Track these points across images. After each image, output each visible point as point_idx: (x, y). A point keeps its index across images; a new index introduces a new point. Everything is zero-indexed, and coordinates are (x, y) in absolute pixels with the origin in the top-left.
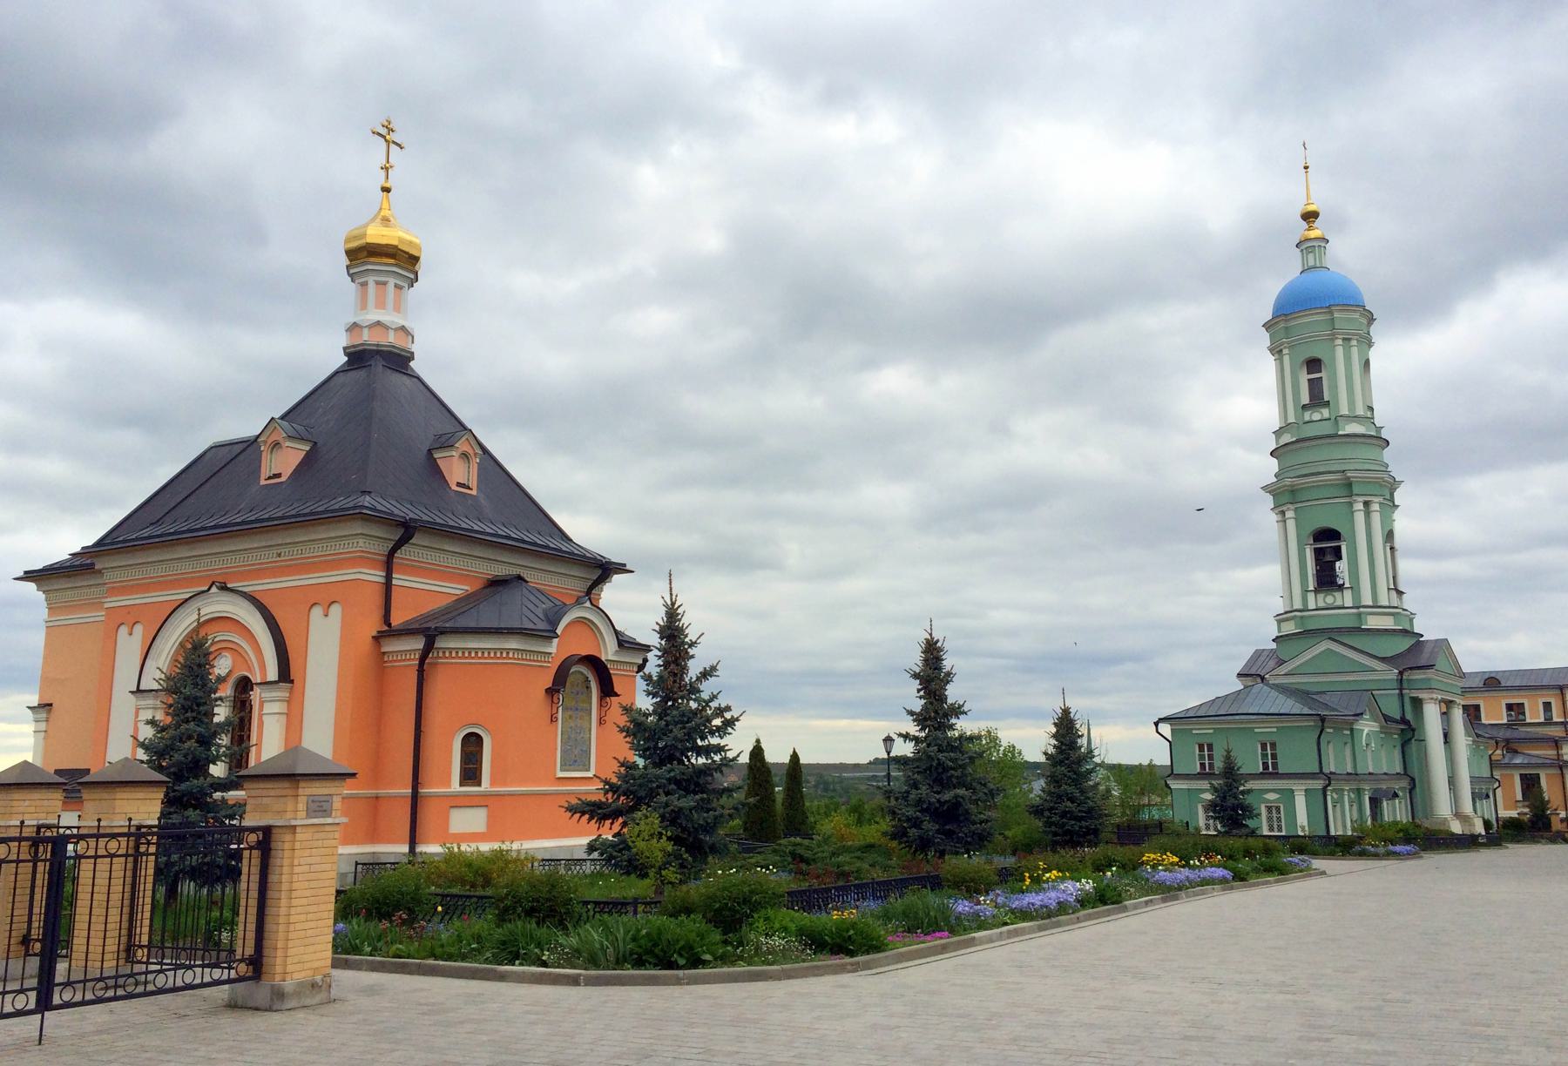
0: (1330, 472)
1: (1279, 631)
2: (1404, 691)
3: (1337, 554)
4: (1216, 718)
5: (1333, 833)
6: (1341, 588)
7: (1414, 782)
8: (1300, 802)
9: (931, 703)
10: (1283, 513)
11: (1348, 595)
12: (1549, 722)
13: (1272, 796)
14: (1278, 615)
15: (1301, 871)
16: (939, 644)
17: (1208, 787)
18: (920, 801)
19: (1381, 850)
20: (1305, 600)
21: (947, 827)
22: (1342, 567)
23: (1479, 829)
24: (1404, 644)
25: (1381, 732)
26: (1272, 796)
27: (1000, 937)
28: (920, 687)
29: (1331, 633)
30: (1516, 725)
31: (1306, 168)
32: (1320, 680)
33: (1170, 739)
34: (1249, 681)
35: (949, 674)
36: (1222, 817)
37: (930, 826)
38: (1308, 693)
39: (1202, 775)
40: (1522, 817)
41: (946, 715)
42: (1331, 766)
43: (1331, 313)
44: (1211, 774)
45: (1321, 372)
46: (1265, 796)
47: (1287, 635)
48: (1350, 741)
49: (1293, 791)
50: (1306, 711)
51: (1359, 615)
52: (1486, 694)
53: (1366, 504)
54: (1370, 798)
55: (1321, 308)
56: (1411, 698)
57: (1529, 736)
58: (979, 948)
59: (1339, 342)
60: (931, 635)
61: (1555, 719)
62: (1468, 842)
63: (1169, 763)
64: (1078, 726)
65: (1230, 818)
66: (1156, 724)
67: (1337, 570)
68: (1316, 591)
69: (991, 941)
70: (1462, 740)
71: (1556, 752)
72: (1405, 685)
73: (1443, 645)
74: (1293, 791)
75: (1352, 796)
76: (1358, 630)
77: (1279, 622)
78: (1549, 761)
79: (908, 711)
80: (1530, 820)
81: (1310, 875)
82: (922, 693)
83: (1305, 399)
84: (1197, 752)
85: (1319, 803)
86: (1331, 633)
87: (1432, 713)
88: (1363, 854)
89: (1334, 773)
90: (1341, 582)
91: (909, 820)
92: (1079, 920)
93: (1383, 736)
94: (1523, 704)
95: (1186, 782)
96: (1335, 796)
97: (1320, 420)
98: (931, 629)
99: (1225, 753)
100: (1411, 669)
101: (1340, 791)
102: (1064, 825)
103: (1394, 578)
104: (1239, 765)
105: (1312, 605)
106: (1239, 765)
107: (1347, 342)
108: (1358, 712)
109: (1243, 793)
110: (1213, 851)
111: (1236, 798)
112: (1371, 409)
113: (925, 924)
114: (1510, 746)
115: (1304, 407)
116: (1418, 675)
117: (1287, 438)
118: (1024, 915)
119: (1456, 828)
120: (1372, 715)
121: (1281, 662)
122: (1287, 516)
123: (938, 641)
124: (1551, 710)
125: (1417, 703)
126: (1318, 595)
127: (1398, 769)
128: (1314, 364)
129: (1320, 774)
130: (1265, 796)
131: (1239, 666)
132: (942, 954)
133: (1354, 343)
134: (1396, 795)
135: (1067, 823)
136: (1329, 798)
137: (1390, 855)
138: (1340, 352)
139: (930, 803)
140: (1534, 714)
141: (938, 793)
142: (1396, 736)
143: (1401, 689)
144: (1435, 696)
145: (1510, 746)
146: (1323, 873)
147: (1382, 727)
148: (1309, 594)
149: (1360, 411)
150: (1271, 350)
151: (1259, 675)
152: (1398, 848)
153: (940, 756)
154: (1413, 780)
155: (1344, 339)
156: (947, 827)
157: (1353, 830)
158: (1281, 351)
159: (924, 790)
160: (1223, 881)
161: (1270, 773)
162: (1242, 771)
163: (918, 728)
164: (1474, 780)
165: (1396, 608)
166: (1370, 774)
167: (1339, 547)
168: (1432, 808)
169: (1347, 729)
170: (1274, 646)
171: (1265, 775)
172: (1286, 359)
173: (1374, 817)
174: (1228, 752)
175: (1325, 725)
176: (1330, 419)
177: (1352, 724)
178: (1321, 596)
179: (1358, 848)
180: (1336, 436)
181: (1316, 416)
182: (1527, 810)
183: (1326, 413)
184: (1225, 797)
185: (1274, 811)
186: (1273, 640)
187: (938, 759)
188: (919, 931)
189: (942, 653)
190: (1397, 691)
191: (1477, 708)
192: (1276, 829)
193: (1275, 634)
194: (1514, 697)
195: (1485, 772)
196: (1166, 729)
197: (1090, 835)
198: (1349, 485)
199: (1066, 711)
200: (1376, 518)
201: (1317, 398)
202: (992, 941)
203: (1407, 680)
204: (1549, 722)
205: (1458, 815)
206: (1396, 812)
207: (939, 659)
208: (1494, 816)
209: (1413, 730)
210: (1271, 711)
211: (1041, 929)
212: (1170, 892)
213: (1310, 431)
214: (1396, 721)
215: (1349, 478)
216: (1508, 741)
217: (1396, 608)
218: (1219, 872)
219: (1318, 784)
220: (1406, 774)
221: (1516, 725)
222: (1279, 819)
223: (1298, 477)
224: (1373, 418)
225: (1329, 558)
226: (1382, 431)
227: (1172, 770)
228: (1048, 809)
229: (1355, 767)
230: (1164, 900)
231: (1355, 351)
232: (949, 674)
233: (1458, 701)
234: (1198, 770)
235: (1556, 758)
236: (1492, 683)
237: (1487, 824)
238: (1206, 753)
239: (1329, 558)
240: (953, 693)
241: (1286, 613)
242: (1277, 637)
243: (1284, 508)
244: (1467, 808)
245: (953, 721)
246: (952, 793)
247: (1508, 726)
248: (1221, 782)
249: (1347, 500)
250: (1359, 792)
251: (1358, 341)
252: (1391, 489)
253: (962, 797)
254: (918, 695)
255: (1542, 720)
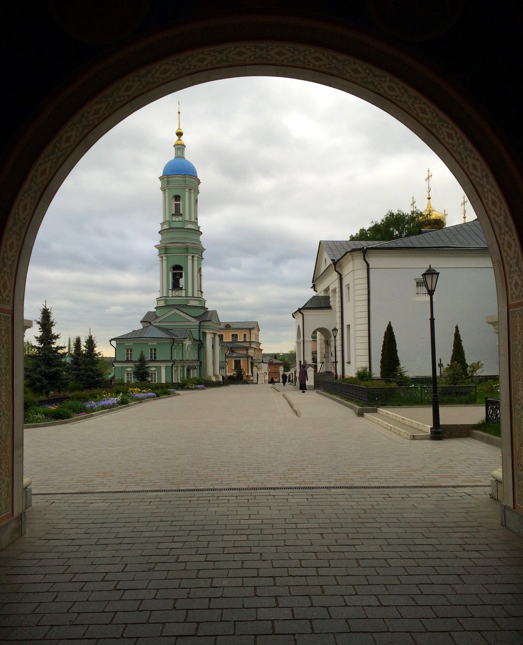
0: (181, 243)
1: (158, 304)
2: (201, 330)
3: (181, 275)
4: (135, 339)
5: (174, 382)
6: (181, 289)
7: (201, 362)
8: (163, 371)
9: (46, 334)
10: (162, 257)
11: (184, 291)
12: (245, 341)
13: (129, 369)
14: (157, 298)
15: (173, 394)
16: (49, 311)
17: (133, 366)
18: (41, 372)
19: (193, 387)
20: (168, 293)
21: (52, 382)
22: (182, 281)
23: (221, 379)
24: (202, 312)
25: (192, 345)
26: (129, 369)
27: (99, 414)
28: (40, 327)
29: (177, 307)
30: (234, 342)
31: (179, 113)
32: (172, 324)
33: (116, 347)
34: (146, 325)
35: (52, 322)
36: (138, 377)
37: (45, 381)
38: (167, 329)
39: (128, 361)
40: (234, 375)
41: (51, 339)
42: (175, 358)
43: (185, 177)
44: (155, 360)
45: (180, 201)
46: (126, 369)
47: (160, 306)
48: (182, 348)
49: (161, 367)
50: (168, 336)
51: (187, 300)
52: (226, 331)
53: (193, 257)
54: (187, 369)
55: (181, 175)
56: (203, 332)
57: (239, 346)
58: (94, 417)
59: (187, 190)
60: (45, 307)
61: (247, 340)
62: (217, 384)
63: (115, 357)
64: (95, 343)
65: (141, 377)
66: (110, 341)
67: (180, 282)
68: (172, 290)
69: (97, 415)
70: (218, 347)
71: (246, 352)
72: (201, 328)
73: (214, 312)
74: (161, 367)
75: (181, 368)
76: (186, 306)
77: (158, 301)
78: (244, 355)
79: (35, 337)
80: (237, 376)
81: (176, 395)
82: (41, 330)
83: (174, 213)
84: (126, 352)
85: (170, 371)
86: (177, 307)
87: (209, 337)
88: (188, 389)
89: (176, 360)
90: (181, 286)
91: (36, 379)
92: (118, 409)
93: (192, 346)
94: (237, 334)
95: (121, 364)
96: (175, 368)
97: (178, 221)
98: (46, 304)
99: (141, 353)
100: (204, 321)
101: (177, 367)
102: (88, 380)
103: (200, 286)
104: (146, 357)
105: (170, 295)
106: (146, 357)
107: (190, 191)
108: (185, 337)
109: (146, 367)
110: (147, 388)
111: (144, 370)
112: (197, 219)
113: (77, 411)
114: (232, 350)
115: (173, 215)
116: (206, 324)
117: (166, 227)
118: (103, 408)
119: (214, 379)
120: (189, 338)
121: (157, 317)
122: (163, 259)
123: (48, 309)
124: (246, 337)
125: (205, 334)
126: (173, 291)
127: (197, 358)
128: (177, 198)
129: (171, 360)
130: (126, 369)
131: (142, 317)
132: (86, 419)
133: (193, 191)
134: (195, 368)
135: (89, 380)
136: (173, 369)
137: (196, 389)
138: (187, 193)
139: (46, 373)
140: (240, 339)
141: (48, 369)
142: (197, 346)
143: (200, 329)
144: (211, 331)
145: (232, 350)
146: (179, 394)
147: (192, 343)
148: (170, 291)
149: (193, 220)
150: (161, 189)
151: (149, 322)
152: (199, 386)
153: (50, 355)
154: (201, 362)
155: (189, 189)
156: (52, 382)
157: (181, 381)
158: (165, 190)
159: (43, 368)
160: (153, 397)
161: (153, 360)
162: (146, 360)
163: (39, 344)
164: (221, 362)
165: (200, 298)
166: (187, 360)
167: (182, 273)
168: (206, 371)
169: (181, 344)
170: (155, 310)
171: (151, 361)
172: (167, 193)
173: (187, 377)
174: (142, 352)
175: (175, 342)
176: (182, 221)
177: (183, 342)
178: (174, 292)
179: (186, 387)
180: (184, 228)
181: (177, 219)
182: (236, 373)
183: (181, 218)
184: (140, 370)
185: (129, 375)
186: (155, 308)
187: (49, 356)
188: (75, 413)
189: (50, 314)
190: (198, 330)
191: (222, 335)
192: (153, 381)
193: (156, 306)
194: (235, 332)
195: (224, 359)
196: (114, 343)
197: (98, 384)
198: (187, 249)
199: (91, 337)
200: (196, 262)
201: (177, 213)
202: (97, 415)
203: (202, 325)
204: (245, 341)
205: (214, 375)
206: (194, 374)
207: (49, 317)
208: (225, 375)
209: (203, 344)
210: (155, 337)
211: (109, 412)
212: (140, 400)
213: (174, 225)
214: (197, 341)
215: (187, 246)
216: (231, 348)
217: (200, 298)
218: (152, 394)
219: (170, 364)
220: (199, 360)
221: (234, 342)
222: (155, 378)
223: (168, 243)
224: (197, 223)
225: (178, 277)
226: (200, 228)
227: (116, 360)
228: (82, 375)
229: (183, 358)
230: (139, 403)
231: (193, 195)
232: (52, 322)
233: (218, 333)
234: (150, 359)
235: (246, 354)
236: (228, 327)
237: (223, 377)
238: (129, 352)
239: (178, 277)
240: (55, 331)
241: (161, 297)
242: (157, 307)
243: (163, 255)
244: (217, 373)
245: (54, 341)
246: (55, 369)
247: (232, 342)
248: (138, 364)
249: (186, 254)
250: (183, 367)
251: (194, 191)
252: (202, 251)
253: (59, 370)
254: (40, 330)
255: (243, 340)
